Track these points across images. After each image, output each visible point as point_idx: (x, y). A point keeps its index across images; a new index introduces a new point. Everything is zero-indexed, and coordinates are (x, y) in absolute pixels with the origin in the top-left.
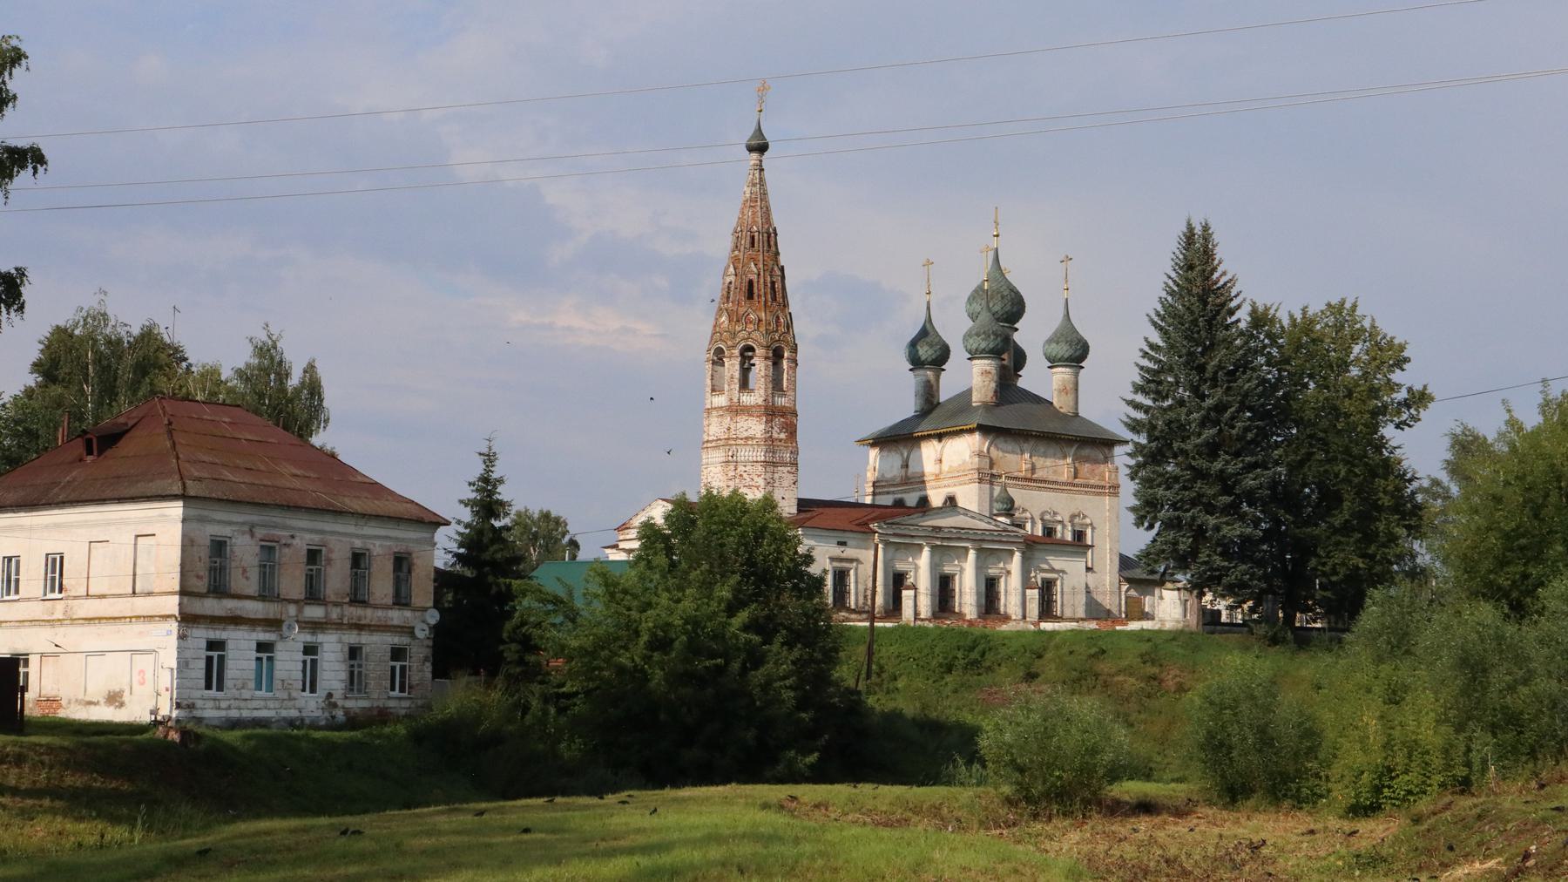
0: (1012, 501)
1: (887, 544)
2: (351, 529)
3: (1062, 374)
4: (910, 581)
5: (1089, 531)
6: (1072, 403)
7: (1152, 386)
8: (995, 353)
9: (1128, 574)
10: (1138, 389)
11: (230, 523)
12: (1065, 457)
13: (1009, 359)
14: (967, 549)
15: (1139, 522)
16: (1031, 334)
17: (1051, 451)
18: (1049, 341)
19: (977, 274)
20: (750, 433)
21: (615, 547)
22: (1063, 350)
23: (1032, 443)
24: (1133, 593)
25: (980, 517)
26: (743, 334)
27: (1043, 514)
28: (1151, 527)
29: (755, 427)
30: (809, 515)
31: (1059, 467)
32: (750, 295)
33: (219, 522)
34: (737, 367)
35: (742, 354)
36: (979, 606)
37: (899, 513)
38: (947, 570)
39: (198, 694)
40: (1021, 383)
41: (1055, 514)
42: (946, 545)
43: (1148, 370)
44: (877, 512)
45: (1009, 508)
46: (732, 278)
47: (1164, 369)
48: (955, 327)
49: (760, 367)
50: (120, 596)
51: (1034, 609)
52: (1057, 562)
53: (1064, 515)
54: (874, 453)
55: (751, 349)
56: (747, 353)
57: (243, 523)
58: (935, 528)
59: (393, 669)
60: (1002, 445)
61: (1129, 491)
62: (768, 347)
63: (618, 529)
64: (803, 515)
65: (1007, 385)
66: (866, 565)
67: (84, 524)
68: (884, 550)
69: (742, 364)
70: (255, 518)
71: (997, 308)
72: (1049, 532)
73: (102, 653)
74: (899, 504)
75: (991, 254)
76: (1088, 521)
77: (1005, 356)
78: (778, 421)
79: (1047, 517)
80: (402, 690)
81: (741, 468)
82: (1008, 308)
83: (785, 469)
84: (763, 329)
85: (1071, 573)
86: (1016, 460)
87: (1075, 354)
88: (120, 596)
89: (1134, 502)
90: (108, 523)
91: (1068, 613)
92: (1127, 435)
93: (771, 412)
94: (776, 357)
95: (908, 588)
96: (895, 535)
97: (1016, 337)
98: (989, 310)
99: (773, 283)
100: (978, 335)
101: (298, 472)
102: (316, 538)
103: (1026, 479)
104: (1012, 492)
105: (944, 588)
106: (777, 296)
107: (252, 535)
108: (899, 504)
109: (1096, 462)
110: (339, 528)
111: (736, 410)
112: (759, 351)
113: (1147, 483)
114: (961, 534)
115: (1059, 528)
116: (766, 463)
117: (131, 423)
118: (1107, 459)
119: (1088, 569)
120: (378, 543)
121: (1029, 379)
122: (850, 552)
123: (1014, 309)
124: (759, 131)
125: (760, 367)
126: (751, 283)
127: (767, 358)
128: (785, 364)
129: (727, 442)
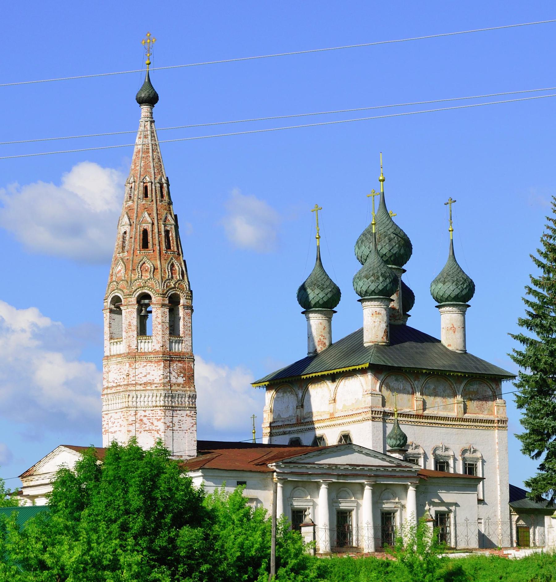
0: (405, 438)
1: (285, 482)
3: (449, 317)
4: (307, 520)
5: (479, 464)
6: (460, 341)
7: (538, 321)
8: (384, 295)
9: (516, 504)
10: (524, 323)
12: (455, 395)
13: (394, 292)
14: (362, 486)
15: (527, 449)
16: (418, 274)
17: (440, 389)
18: (436, 281)
19: (367, 217)
20: (150, 378)
21: (20, 493)
22: (449, 289)
23: (422, 380)
24: (521, 523)
26: (141, 282)
28: (538, 455)
29: (155, 372)
30: (208, 456)
32: (145, 245)
34: (135, 314)
35: (138, 302)
36: (376, 538)
37: (295, 450)
38: (344, 505)
40: (410, 323)
41: (447, 449)
42: (342, 484)
43: (532, 305)
44: (275, 451)
45: (402, 445)
46: (127, 228)
47: (545, 303)
48: (346, 272)
49: (158, 316)
50: (314, 533)
51: (429, 538)
52: (448, 497)
53: (455, 450)
54: (269, 395)
55: (148, 297)
56: (143, 300)
58: (330, 466)
60: (393, 384)
61: (516, 416)
62: (164, 295)
63: (22, 476)
65: (399, 331)
66: (268, 500)
68: (283, 489)
69: (139, 311)
71: (384, 251)
72: (441, 464)
74: (295, 443)
75: (378, 199)
76: (478, 455)
77: (394, 297)
78: (176, 366)
81: (141, 413)
82: (395, 250)
83: (184, 413)
84: (158, 276)
85: (463, 504)
86: (410, 403)
87: (462, 295)
88: (314, 533)
89: (523, 430)
91: (461, 546)
92: (514, 368)
93: (168, 358)
94: (173, 303)
95: (307, 525)
97: (404, 278)
98: (378, 252)
99: (167, 232)
100: (367, 277)
103: (418, 416)
104: (405, 429)
105: (341, 523)
106: (172, 244)
108: (295, 443)
109: (485, 399)
111: (134, 356)
112: (155, 299)
113: (534, 413)
114: (356, 471)
115: (451, 462)
116: (166, 408)
118: (495, 395)
119: (481, 502)
121: (416, 320)
122: (247, 493)
123: (401, 252)
125: (158, 316)
126: (145, 232)
127: (163, 305)
128: (181, 312)
129: (130, 387)
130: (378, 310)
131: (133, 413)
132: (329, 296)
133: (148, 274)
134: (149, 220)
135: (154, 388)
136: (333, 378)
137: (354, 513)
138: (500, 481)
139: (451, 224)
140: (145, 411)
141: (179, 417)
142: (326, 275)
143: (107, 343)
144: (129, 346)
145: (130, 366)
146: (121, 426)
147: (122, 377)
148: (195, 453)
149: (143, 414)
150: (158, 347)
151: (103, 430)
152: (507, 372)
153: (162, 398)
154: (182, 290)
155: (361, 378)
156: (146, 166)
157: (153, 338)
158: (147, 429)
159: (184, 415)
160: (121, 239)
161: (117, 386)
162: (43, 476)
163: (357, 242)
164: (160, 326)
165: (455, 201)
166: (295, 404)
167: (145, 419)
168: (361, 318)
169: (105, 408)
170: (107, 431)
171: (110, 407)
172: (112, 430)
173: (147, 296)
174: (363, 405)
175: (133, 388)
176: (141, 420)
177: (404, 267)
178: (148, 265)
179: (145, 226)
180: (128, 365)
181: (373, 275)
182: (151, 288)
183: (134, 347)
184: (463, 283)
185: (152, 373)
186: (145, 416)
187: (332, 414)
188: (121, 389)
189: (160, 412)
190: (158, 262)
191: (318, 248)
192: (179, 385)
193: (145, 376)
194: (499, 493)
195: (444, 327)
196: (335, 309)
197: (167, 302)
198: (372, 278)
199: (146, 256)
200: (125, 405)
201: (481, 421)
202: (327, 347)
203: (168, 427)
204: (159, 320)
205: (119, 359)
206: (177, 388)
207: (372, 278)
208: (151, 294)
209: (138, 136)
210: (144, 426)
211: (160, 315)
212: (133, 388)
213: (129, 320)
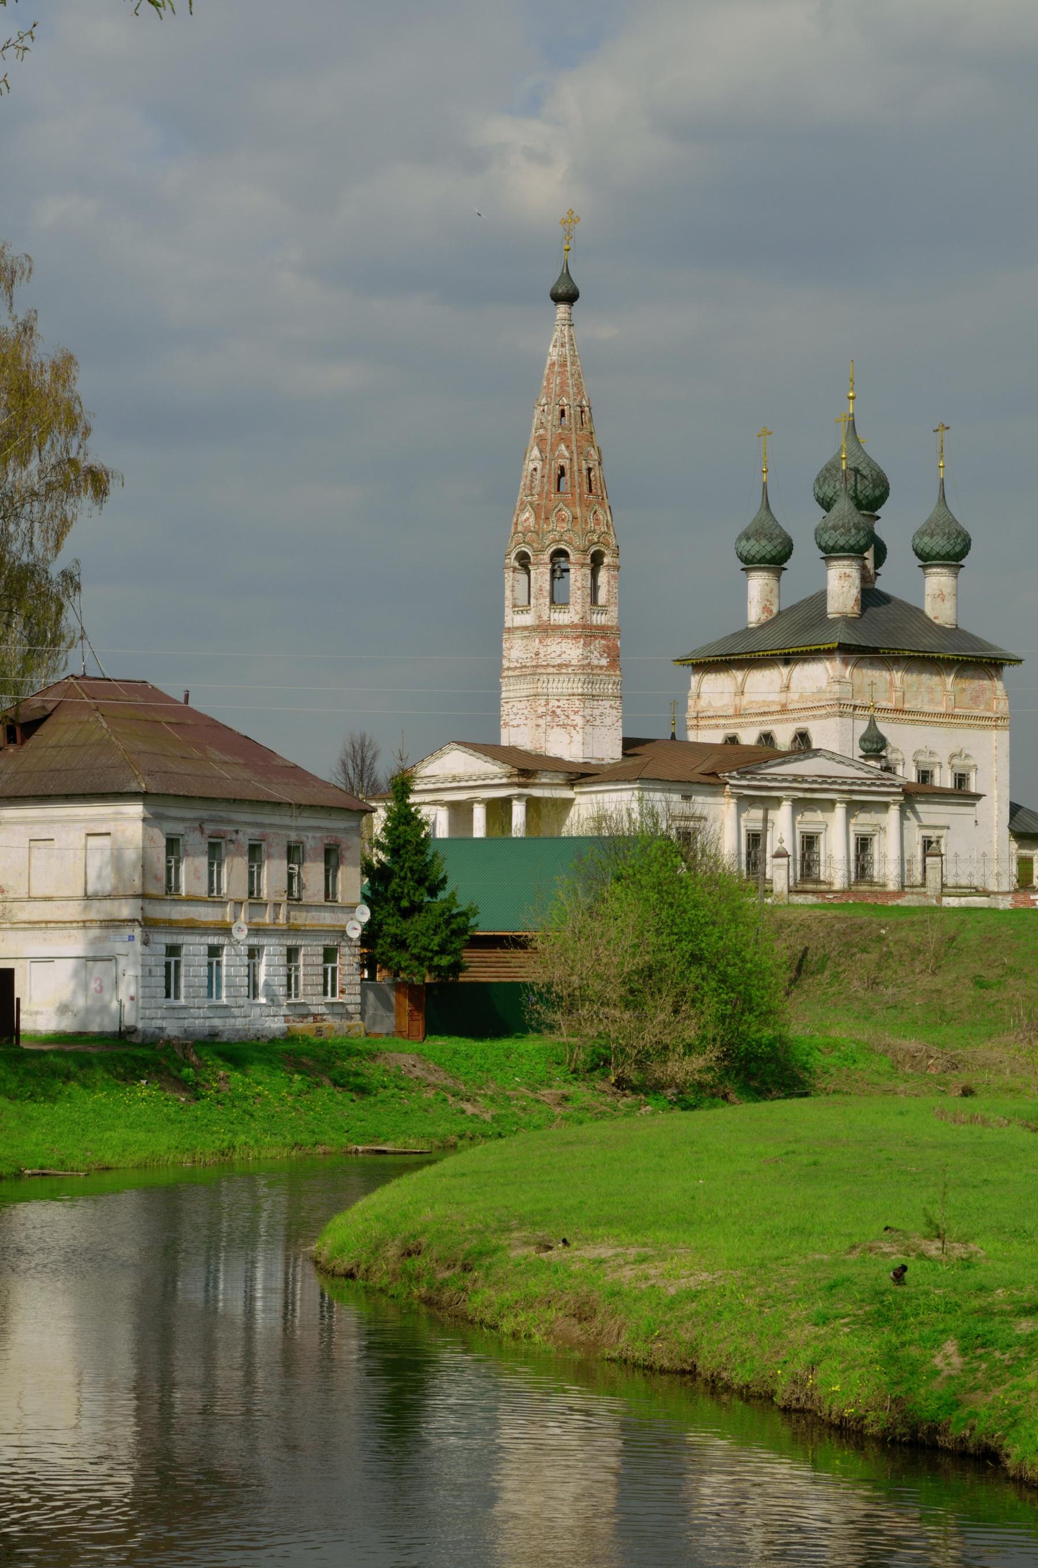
2: (287, 821)
3: (938, 582)
8: (855, 552)
11: (183, 820)
22: (938, 544)
25: (850, 762)
27: (918, 753)
31: (937, 690)
33: (175, 819)
39: (315, 1000)
46: (539, 465)
49: (577, 577)
57: (195, 819)
59: (326, 970)
62: (585, 551)
64: (631, 762)
67: (24, 822)
70: (204, 814)
72: (925, 776)
73: (50, 959)
79: (920, 758)
80: (333, 995)
83: (607, 704)
86: (888, 684)
90: (52, 821)
96: (749, 787)
97: (877, 532)
101: (227, 758)
102: (256, 832)
104: (883, 728)
107: (202, 831)
110: (276, 819)
111: (545, 630)
117: (50, 707)
120: (310, 835)
123: (871, 497)
124: (566, 276)
130: (848, 571)
131: (543, 702)
132: (779, 548)
133: (564, 525)
134: (567, 454)
135: (570, 671)
136: (788, 660)
137: (822, 837)
138: (998, 796)
139: (942, 457)
140: (558, 700)
141: (601, 709)
142: (775, 520)
143: (508, 611)
144: (540, 617)
145: (541, 642)
146: (527, 719)
147: (529, 656)
148: (620, 756)
149: (556, 703)
150: (576, 619)
151: (502, 722)
152: (992, 648)
153: (580, 685)
154: (607, 545)
155: (828, 664)
156: (563, 385)
157: (571, 607)
158: (561, 723)
159: (607, 706)
160: (529, 478)
161: (521, 668)
162: (426, 780)
163: (818, 479)
164: (579, 592)
165: (948, 428)
166: (733, 689)
167: (558, 711)
168: (825, 580)
169: (504, 695)
170: (506, 724)
171: (511, 694)
172: (515, 723)
173: (561, 553)
174: (828, 696)
175: (543, 671)
176: (553, 712)
177: (878, 513)
178: (566, 513)
179: (561, 462)
180: (537, 641)
181: (843, 526)
182: (569, 543)
183: (545, 618)
184: (957, 537)
185: (568, 652)
186: (559, 707)
187: (784, 705)
188: (528, 671)
189: (577, 702)
190: (578, 510)
191: (765, 485)
192: (601, 667)
193: (560, 656)
194: (996, 812)
195: (937, 596)
196: (785, 566)
197: (589, 561)
198: (842, 530)
199: (563, 501)
200: (532, 692)
201: (976, 718)
202: (774, 615)
203: (588, 721)
204: (579, 584)
205: (526, 633)
206: (599, 672)
207: (842, 530)
208: (569, 551)
209: (552, 343)
210: (557, 720)
211: (579, 578)
212: (543, 671)
213: (539, 584)
